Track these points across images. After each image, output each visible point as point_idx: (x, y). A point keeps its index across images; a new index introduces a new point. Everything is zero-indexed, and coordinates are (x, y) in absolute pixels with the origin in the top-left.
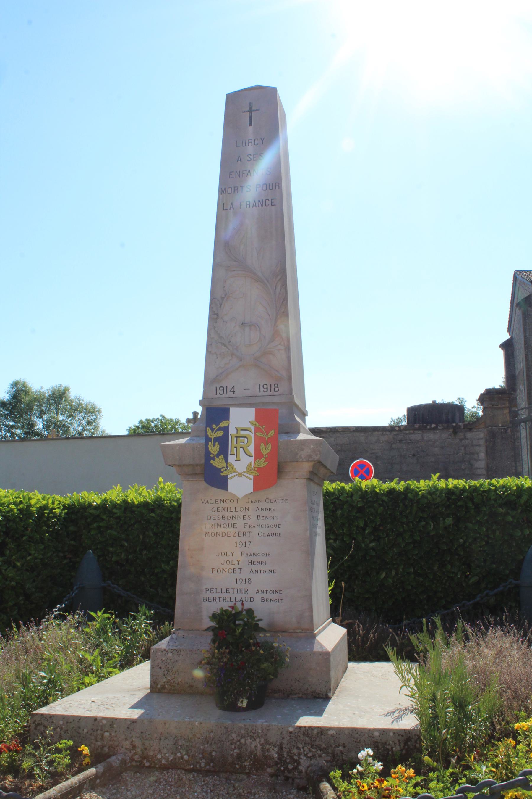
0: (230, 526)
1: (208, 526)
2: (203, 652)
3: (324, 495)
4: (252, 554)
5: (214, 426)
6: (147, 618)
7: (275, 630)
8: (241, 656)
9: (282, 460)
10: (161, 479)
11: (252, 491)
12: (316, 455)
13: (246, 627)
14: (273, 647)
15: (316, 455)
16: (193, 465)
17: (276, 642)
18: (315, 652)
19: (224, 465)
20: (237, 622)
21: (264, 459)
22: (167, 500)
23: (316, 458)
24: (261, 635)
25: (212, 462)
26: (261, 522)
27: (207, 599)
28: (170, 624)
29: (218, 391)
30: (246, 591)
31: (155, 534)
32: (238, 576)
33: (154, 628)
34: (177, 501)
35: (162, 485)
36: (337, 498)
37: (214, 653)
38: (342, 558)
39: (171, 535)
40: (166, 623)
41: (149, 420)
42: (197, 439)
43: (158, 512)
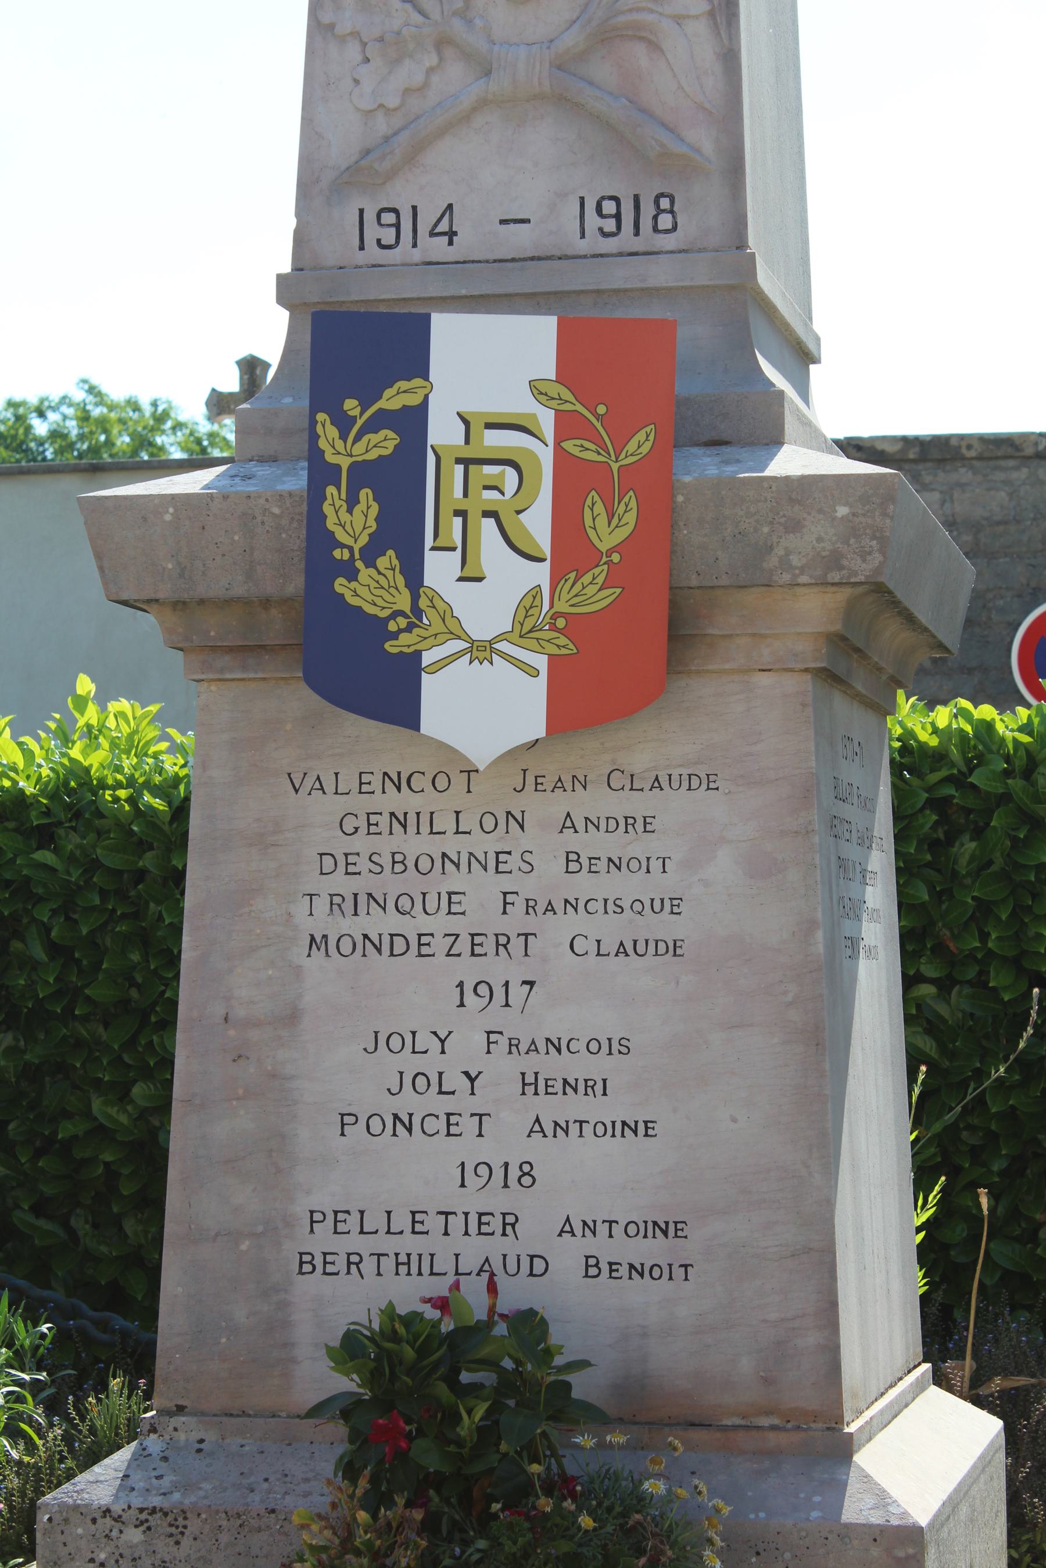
1: (321, 905)
2: (296, 1519)
3: (897, 769)
4: (541, 1045)
5: (351, 405)
6: (18, 1360)
7: (652, 1413)
8: (482, 1544)
9: (694, 582)
10: (85, 685)
11: (541, 733)
12: (864, 554)
13: (511, 1403)
14: (641, 1501)
15: (864, 554)
16: (245, 602)
17: (658, 1476)
18: (848, 1526)
19: (404, 602)
20: (465, 1377)
21: (601, 572)
22: (119, 785)
23: (862, 569)
24: (585, 1441)
25: (340, 585)
26: (583, 886)
27: (318, 1261)
28: (133, 1388)
29: (372, 232)
30: (510, 1224)
31: (54, 949)
32: (468, 1148)
33: (53, 1407)
34: (167, 788)
35: (91, 714)
36: (959, 781)
37: (349, 1528)
38: (980, 1075)
39: (135, 957)
40: (115, 1383)
41: (23, 404)
42: (263, 471)
43: (71, 842)
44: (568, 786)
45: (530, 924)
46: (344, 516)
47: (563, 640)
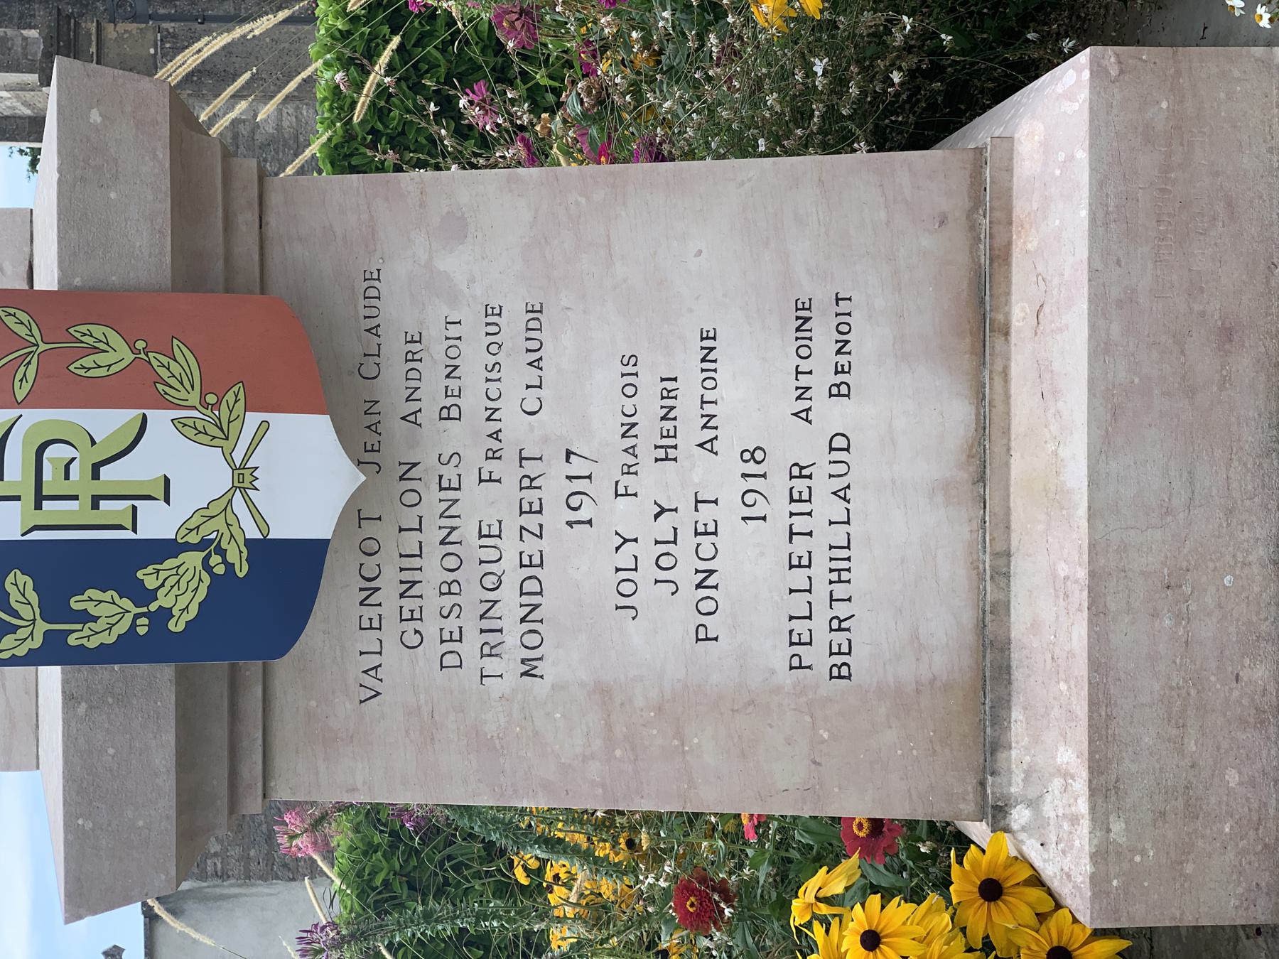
1: (491, 665)
4: (629, 442)
19: (193, 560)
25: (176, 626)
26: (473, 403)
27: (838, 660)
30: (800, 471)
32: (728, 514)
44: (376, 418)
45: (510, 455)
47: (230, 397)
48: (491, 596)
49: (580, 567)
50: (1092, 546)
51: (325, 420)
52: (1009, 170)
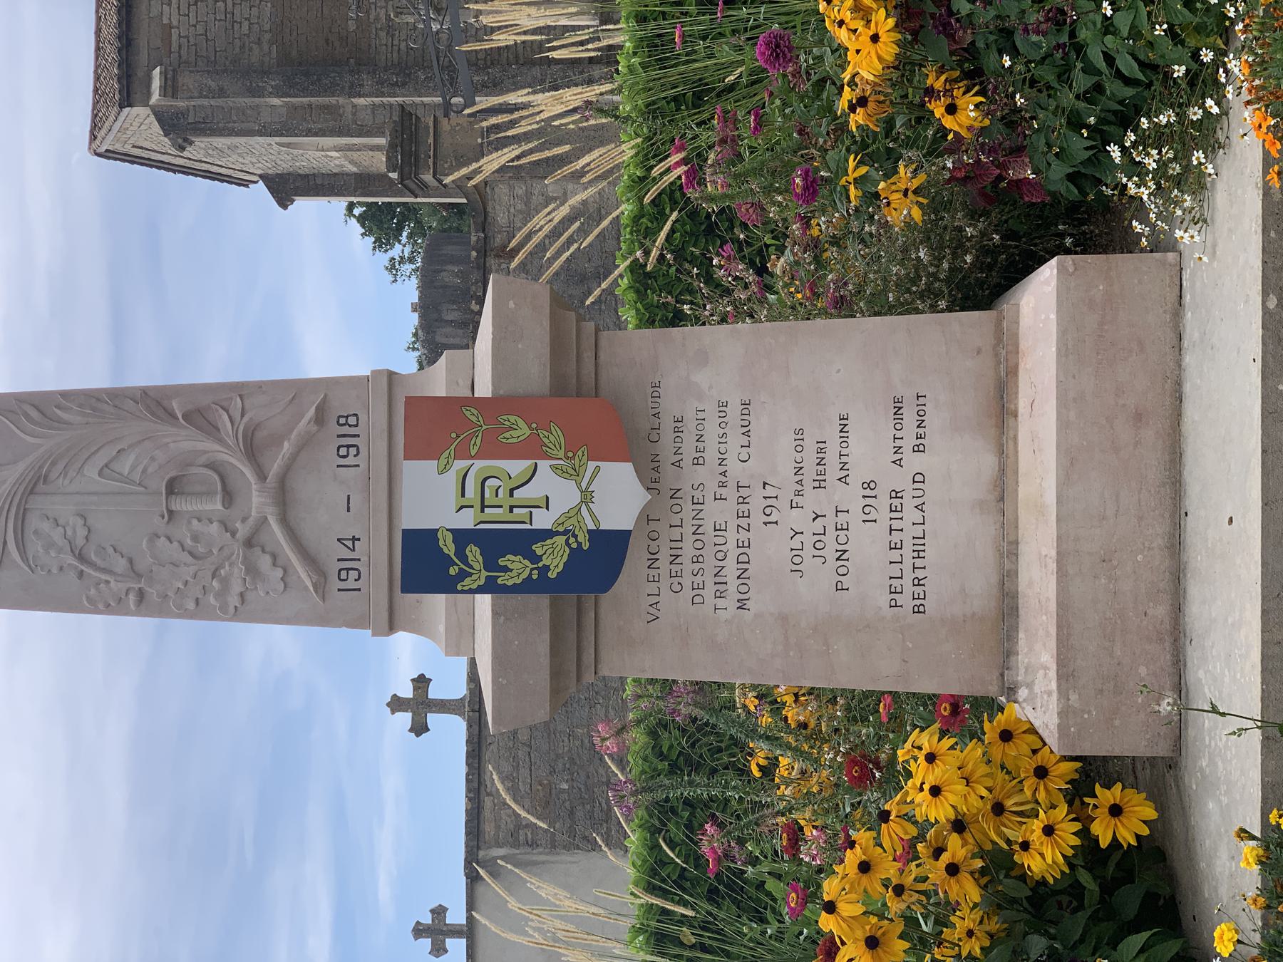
0: (722, 540)
1: (721, 603)
19: (561, 540)
21: (542, 433)
25: (552, 575)
26: (711, 455)
27: (918, 602)
29: (351, 584)
30: (896, 495)
32: (855, 518)
44: (657, 464)
45: (732, 484)
46: (514, 573)
47: (580, 453)
48: (721, 564)
49: (771, 548)
50: (1059, 538)
51: (628, 467)
52: (1018, 323)
